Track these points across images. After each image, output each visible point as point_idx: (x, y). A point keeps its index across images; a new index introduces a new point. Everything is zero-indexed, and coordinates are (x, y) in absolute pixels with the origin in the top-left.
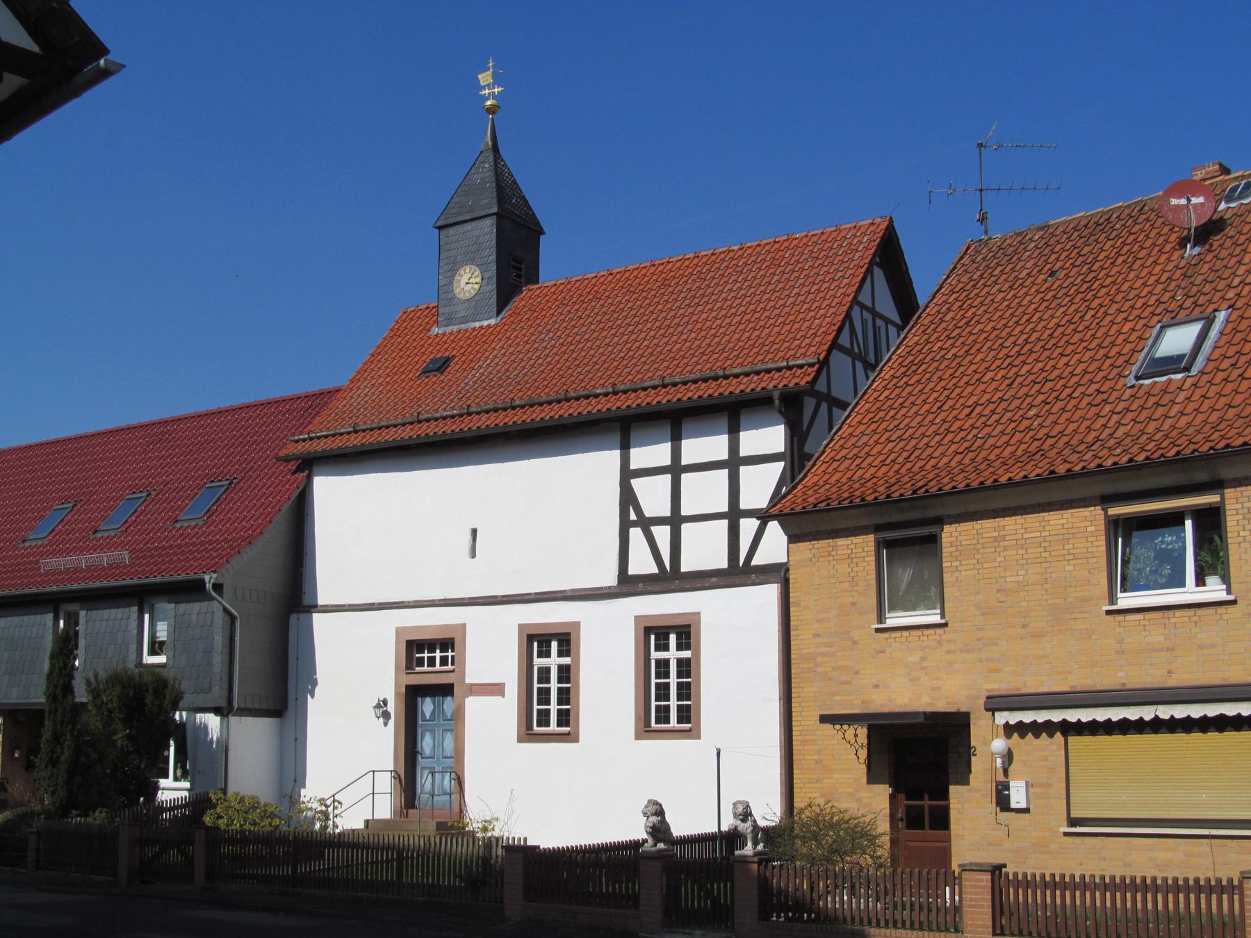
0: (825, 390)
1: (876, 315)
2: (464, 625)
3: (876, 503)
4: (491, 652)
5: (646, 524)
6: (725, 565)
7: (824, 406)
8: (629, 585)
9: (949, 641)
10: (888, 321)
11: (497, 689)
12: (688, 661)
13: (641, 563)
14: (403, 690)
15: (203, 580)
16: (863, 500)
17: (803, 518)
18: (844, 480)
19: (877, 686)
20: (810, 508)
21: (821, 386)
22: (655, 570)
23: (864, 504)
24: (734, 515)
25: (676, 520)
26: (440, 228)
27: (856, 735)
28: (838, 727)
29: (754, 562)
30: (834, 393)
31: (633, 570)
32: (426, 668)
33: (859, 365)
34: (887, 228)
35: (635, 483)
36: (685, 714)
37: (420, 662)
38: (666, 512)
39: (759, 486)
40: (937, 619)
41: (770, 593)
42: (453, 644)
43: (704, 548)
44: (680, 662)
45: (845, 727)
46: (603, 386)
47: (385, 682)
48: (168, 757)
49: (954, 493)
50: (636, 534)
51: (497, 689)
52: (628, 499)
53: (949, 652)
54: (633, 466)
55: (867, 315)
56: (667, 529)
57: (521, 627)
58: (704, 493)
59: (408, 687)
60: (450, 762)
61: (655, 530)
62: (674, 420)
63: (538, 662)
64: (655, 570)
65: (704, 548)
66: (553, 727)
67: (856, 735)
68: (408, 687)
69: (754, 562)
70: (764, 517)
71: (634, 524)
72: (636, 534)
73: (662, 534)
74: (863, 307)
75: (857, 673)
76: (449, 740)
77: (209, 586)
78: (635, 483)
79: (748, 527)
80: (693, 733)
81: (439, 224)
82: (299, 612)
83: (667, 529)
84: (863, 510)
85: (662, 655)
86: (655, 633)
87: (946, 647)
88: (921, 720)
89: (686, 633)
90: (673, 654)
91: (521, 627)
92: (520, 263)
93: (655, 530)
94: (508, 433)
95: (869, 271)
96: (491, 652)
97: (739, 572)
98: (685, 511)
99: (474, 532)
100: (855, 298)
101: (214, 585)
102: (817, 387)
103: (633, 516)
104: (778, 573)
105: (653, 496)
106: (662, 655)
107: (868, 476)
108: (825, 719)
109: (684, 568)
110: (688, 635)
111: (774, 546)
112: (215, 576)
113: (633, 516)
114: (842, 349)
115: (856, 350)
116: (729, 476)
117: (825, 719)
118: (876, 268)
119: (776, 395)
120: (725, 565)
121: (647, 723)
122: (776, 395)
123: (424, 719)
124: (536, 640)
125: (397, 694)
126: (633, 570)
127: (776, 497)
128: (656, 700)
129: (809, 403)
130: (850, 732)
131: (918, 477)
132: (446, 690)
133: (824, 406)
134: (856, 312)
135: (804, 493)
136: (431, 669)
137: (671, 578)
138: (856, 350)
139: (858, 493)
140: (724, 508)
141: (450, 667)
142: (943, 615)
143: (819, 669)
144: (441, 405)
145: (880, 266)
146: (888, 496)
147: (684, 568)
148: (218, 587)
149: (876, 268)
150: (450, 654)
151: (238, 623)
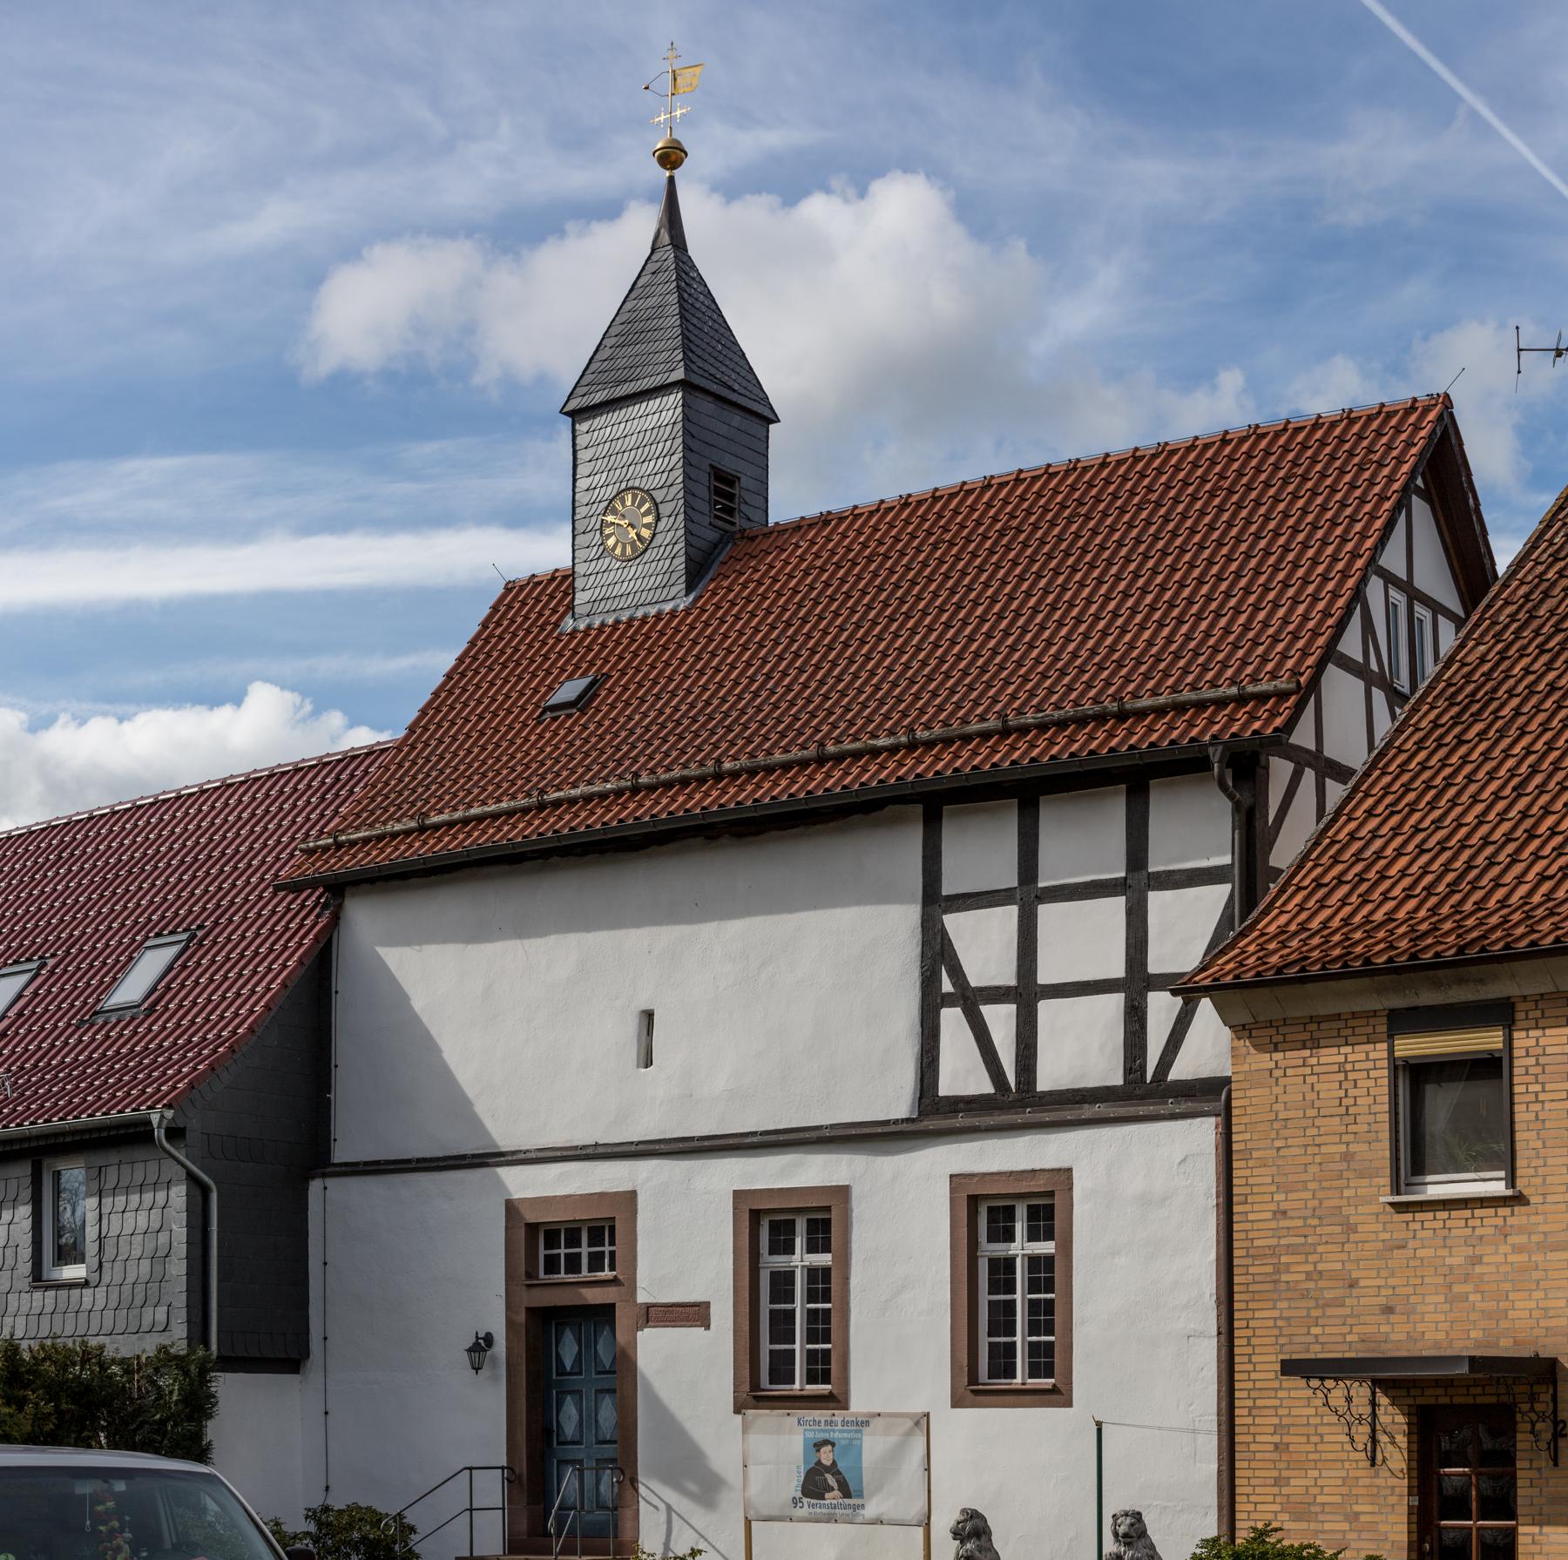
0: (1312, 747)
1: (1415, 596)
2: (633, 1195)
3: (1392, 969)
4: (685, 1244)
5: (971, 1000)
6: (1118, 1080)
7: (1309, 776)
8: (936, 1116)
9: (1521, 1230)
10: (1437, 608)
11: (695, 1314)
12: (1049, 1260)
13: (962, 1073)
14: (521, 1317)
15: (150, 1123)
16: (1368, 961)
17: (1267, 991)
18: (1336, 923)
19: (1388, 1310)
20: (1269, 975)
21: (1303, 736)
22: (987, 1088)
23: (1369, 970)
24: (1136, 983)
25: (1026, 994)
26: (577, 415)
27: (1349, 1399)
28: (1315, 1383)
29: (1173, 1075)
30: (1330, 751)
31: (945, 1088)
32: (585, 1274)
33: (1379, 696)
34: (1440, 417)
35: (951, 921)
36: (1045, 1360)
37: (552, 1265)
38: (1006, 976)
39: (1185, 926)
40: (1498, 1188)
41: (1197, 1136)
42: (612, 1230)
43: (1079, 1045)
44: (1034, 1262)
45: (1330, 1383)
46: (891, 733)
47: (488, 1306)
48: (86, 1443)
49: (1536, 953)
50: (952, 1020)
51: (695, 1314)
52: (937, 952)
53: (1518, 1249)
54: (947, 890)
55: (1397, 597)
56: (1010, 1009)
57: (738, 1194)
58: (1083, 939)
59: (530, 1311)
60: (609, 1451)
61: (987, 1011)
62: (1027, 793)
63: (992, 1250)
64: (987, 1088)
65: (1079, 1045)
66: (798, 1385)
67: (1349, 1399)
68: (530, 1311)
69: (1173, 1075)
70: (1188, 990)
71: (949, 1001)
72: (952, 1020)
73: (1001, 1020)
74: (1389, 579)
75: (1353, 1284)
76: (607, 1413)
77: (160, 1134)
78: (951, 921)
79: (1161, 1008)
80: (1059, 1396)
81: (572, 406)
82: (324, 1176)
83: (1010, 1009)
84: (1366, 980)
85: (1000, 1249)
86: (985, 1211)
87: (1515, 1239)
88: (1464, 1369)
89: (1045, 1206)
90: (801, 1259)
91: (738, 1194)
92: (731, 483)
93: (987, 1011)
94: (711, 826)
95: (1402, 504)
96: (685, 1244)
97: (1144, 1093)
98: (1044, 977)
99: (649, 1016)
100: (1373, 560)
101: (168, 1130)
102: (1295, 739)
103: (947, 986)
104: (1210, 1095)
105: (984, 944)
106: (1000, 1249)
107: (1379, 916)
108: (1290, 1368)
109: (1043, 1085)
110: (1049, 1211)
111: (1208, 1046)
112: (169, 1114)
113: (947, 986)
114: (1346, 664)
115: (1374, 666)
116: (1107, 933)
117: (1290, 1368)
118: (1417, 503)
119: (1215, 754)
120: (1118, 1080)
121: (973, 1378)
122: (1215, 754)
123: (561, 1371)
124: (768, 1225)
125: (510, 1324)
126: (945, 1088)
127: (1217, 947)
128: (1014, 1343)
129: (1280, 770)
130: (1338, 1396)
131: (1470, 922)
132: (605, 1313)
133: (1309, 776)
134: (1375, 587)
135: (1262, 948)
136: (572, 1278)
137: (1018, 1102)
138: (1374, 666)
139: (1359, 949)
140: (1117, 970)
141: (606, 1274)
142: (1511, 1181)
143: (1285, 1277)
144: (587, 790)
145: (1425, 495)
146: (1414, 957)
147: (1043, 1085)
148: (175, 1133)
149: (1417, 503)
150: (607, 1249)
151: (214, 1196)
